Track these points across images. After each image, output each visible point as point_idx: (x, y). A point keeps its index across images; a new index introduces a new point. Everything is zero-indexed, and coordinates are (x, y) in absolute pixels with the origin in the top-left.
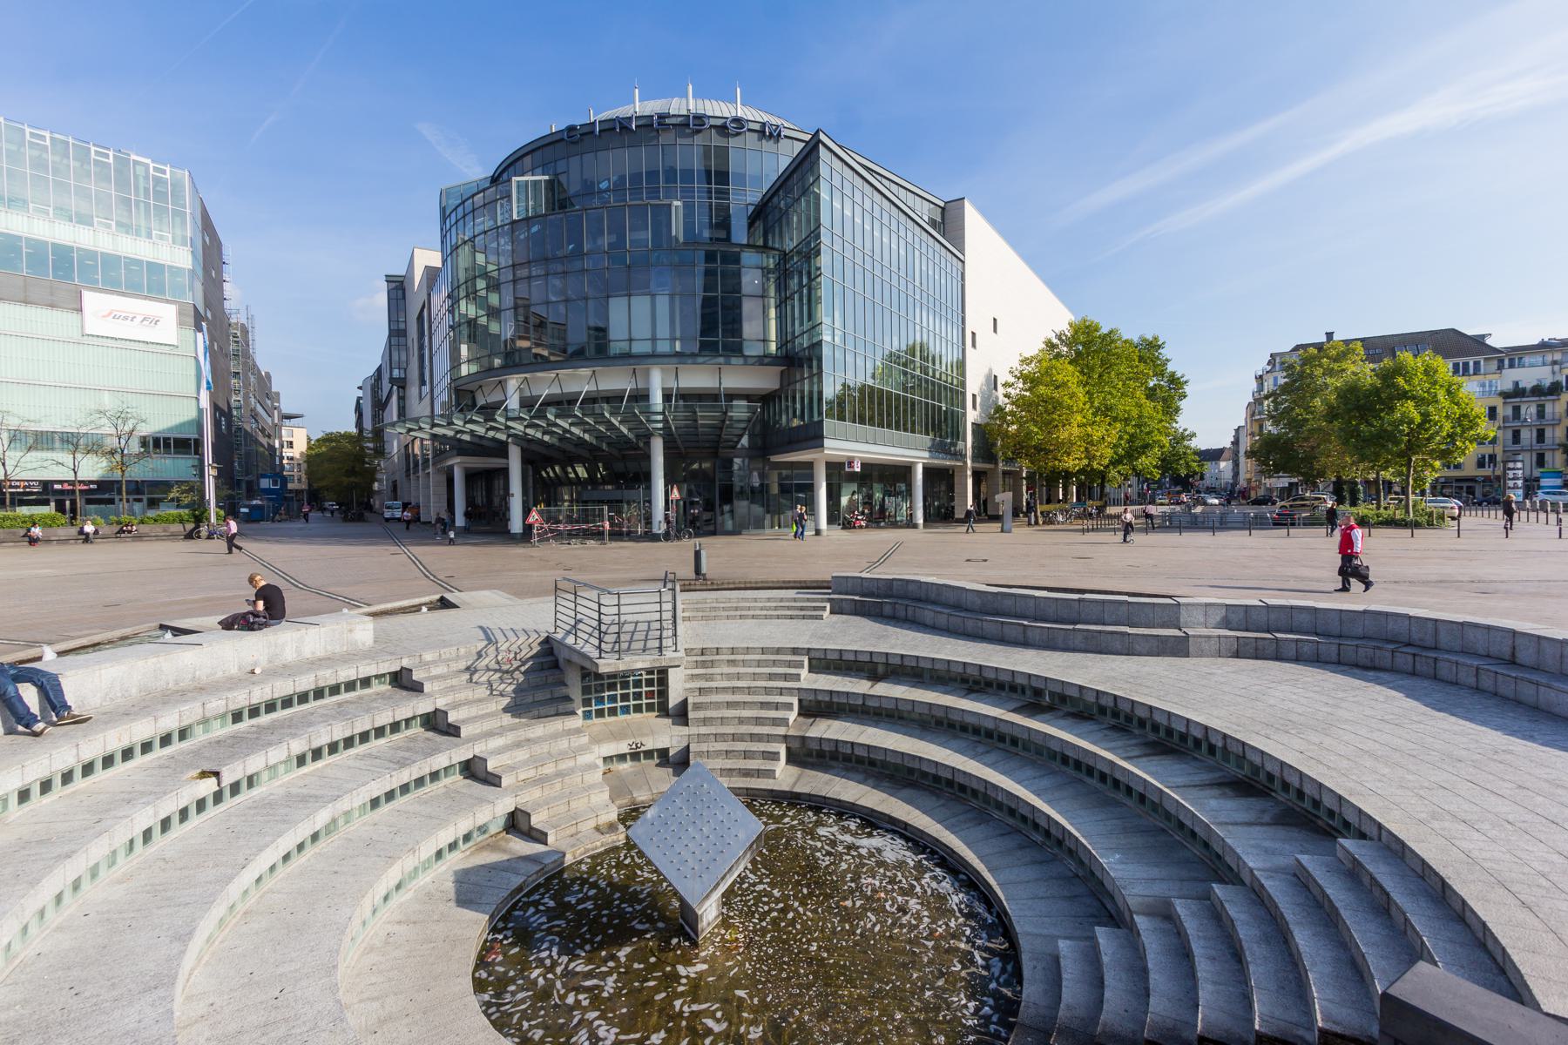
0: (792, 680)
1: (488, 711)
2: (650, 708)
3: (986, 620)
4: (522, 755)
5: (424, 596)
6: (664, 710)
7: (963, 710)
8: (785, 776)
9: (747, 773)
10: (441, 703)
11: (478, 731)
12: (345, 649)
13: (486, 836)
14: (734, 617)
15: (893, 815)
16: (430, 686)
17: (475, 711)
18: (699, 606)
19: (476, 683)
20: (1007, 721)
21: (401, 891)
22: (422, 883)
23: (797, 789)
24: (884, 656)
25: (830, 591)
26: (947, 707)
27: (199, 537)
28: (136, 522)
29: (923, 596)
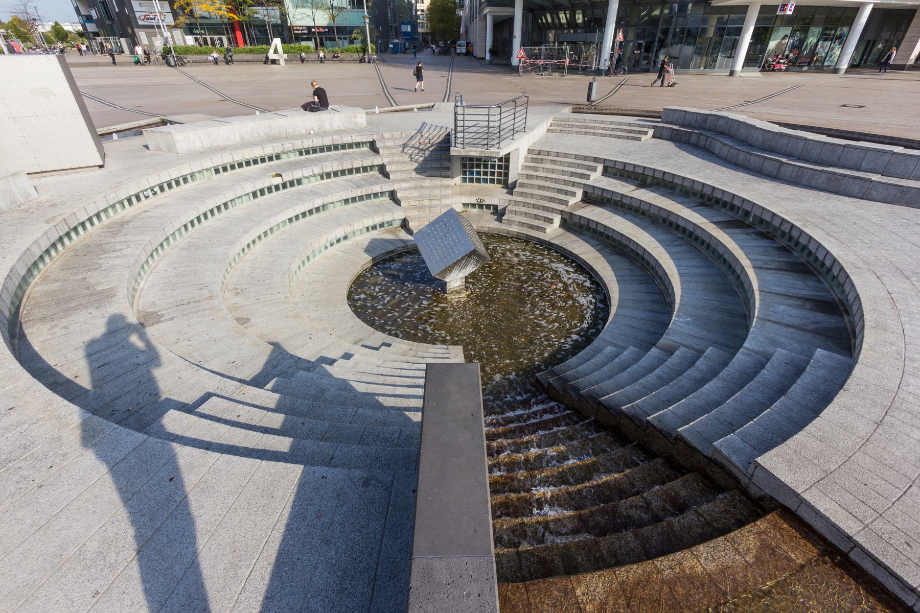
1: (407, 168)
2: (499, 182)
3: (754, 155)
4: (416, 193)
6: (505, 184)
7: (678, 216)
8: (553, 231)
9: (531, 227)
10: (385, 161)
11: (399, 178)
13: (391, 227)
14: (580, 133)
15: (593, 266)
17: (400, 167)
18: (563, 123)
20: (701, 228)
23: (552, 241)
24: (652, 171)
25: (660, 120)
26: (670, 212)
27: (365, 62)
28: (339, 51)
29: (726, 132)
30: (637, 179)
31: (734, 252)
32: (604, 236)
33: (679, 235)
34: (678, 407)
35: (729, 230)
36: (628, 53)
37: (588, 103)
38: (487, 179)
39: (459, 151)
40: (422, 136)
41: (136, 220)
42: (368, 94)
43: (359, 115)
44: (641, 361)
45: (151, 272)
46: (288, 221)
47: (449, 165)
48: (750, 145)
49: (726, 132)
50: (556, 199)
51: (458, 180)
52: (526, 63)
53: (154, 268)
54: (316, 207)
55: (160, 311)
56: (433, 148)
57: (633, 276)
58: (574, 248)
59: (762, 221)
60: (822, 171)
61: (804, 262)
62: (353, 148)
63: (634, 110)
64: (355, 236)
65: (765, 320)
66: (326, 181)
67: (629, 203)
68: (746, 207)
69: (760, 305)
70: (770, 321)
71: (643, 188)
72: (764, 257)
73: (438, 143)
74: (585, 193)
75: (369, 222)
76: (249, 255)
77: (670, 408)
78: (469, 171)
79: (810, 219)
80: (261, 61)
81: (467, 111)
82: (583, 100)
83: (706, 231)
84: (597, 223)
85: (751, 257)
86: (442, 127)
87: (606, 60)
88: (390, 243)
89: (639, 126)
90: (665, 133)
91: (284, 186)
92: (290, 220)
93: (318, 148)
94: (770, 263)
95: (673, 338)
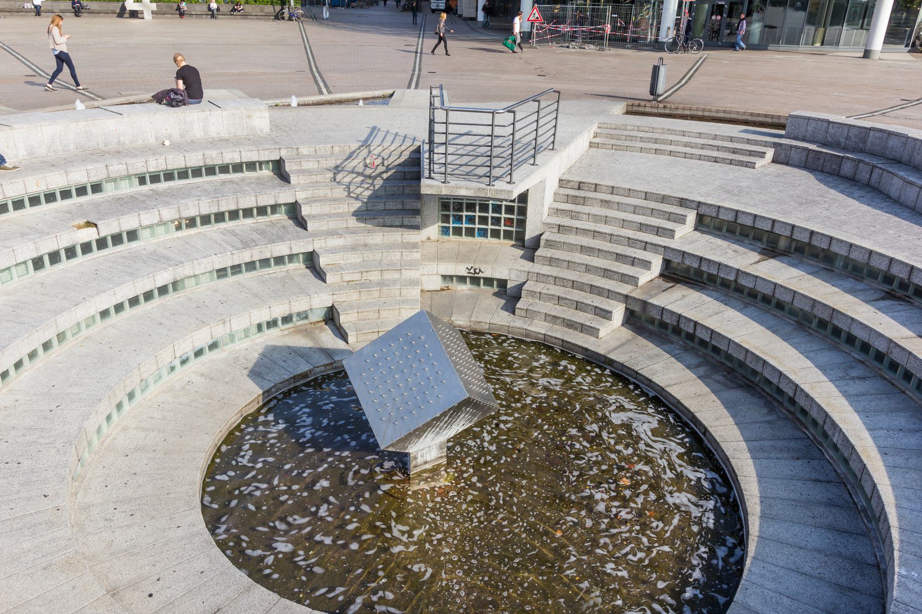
1: (340, 211)
2: (508, 235)
4: (355, 258)
5: (378, 90)
6: (520, 240)
7: (852, 319)
9: (571, 325)
10: (300, 196)
11: (325, 228)
12: (246, 133)
13: (305, 322)
14: (648, 151)
16: (296, 178)
17: (326, 209)
18: (617, 132)
19: (339, 183)
20: (904, 349)
21: (216, 351)
22: (237, 348)
23: (612, 356)
24: (790, 228)
25: (783, 132)
26: (834, 310)
27: (283, 18)
29: (905, 158)
30: (760, 240)
32: (710, 347)
33: (856, 356)
36: (703, 18)
37: (651, 97)
38: (487, 230)
39: (438, 187)
40: (370, 152)
42: (283, 71)
46: (98, 317)
47: (417, 205)
49: (903, 160)
50: (615, 272)
52: (542, 28)
54: (160, 285)
56: (389, 174)
57: (779, 439)
58: (655, 373)
63: (730, 112)
66: (186, 233)
67: (751, 285)
71: (773, 257)
73: (399, 165)
75: (264, 316)
80: (113, 12)
82: (643, 91)
83: (915, 357)
84: (696, 323)
86: (405, 137)
87: (669, 28)
89: (748, 141)
91: (102, 244)
92: (105, 314)
93: (176, 172)
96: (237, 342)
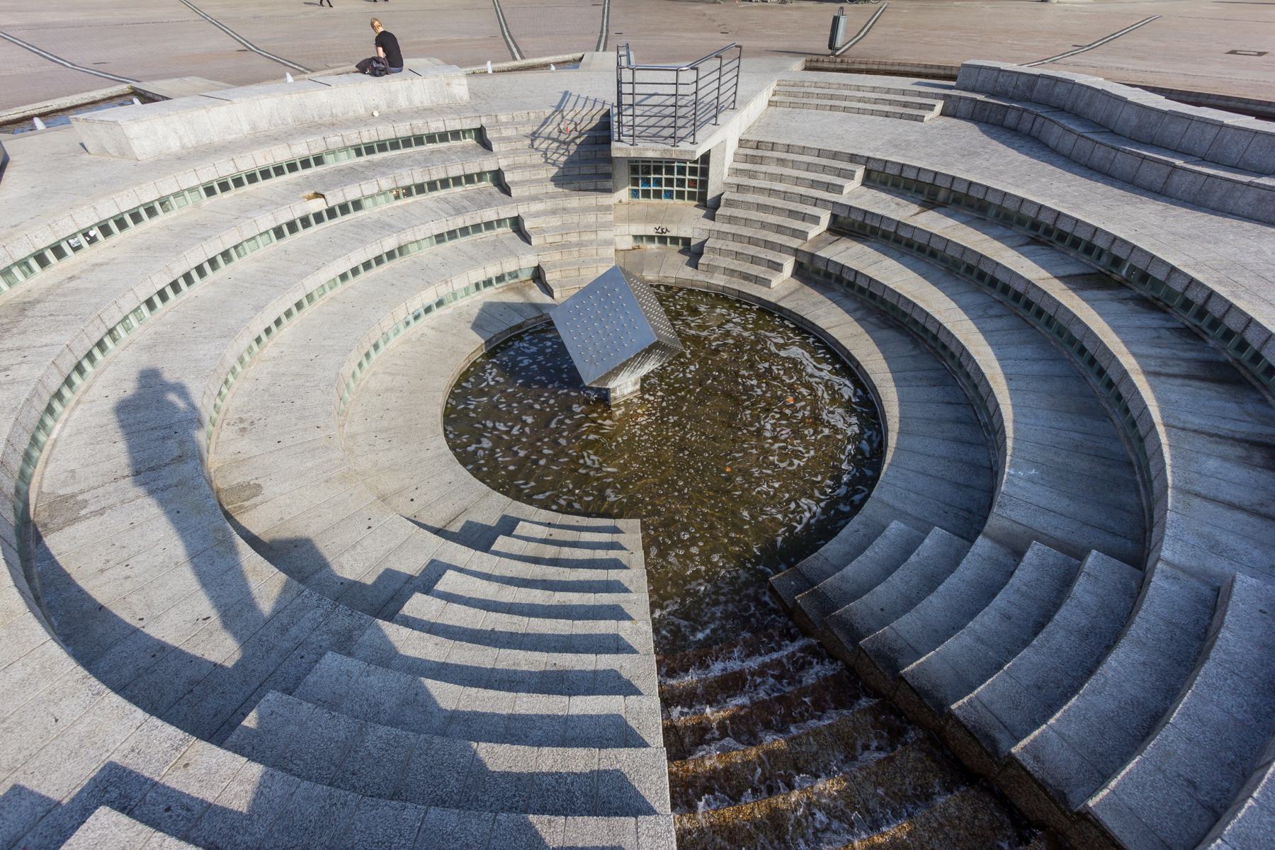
0: (833, 191)
2: (692, 196)
3: (1124, 151)
4: (555, 221)
6: (701, 199)
7: (997, 264)
9: (746, 277)
10: (503, 163)
11: (527, 194)
13: (516, 280)
15: (852, 352)
17: (527, 175)
18: (795, 89)
19: (536, 149)
20: (1040, 289)
23: (782, 304)
26: (982, 256)
30: (921, 192)
31: (1105, 341)
32: (867, 293)
34: (1066, 719)
35: (1089, 293)
39: (627, 149)
40: (563, 117)
41: (51, 297)
42: (477, 37)
43: (456, 81)
44: (961, 568)
45: (78, 402)
48: (1112, 131)
51: (624, 194)
53: (86, 391)
55: (82, 492)
56: (582, 139)
59: (1144, 277)
60: (1249, 184)
61: (1230, 360)
62: (447, 141)
63: (905, 65)
64: (455, 299)
65: (1188, 492)
68: (1117, 251)
69: (1173, 457)
70: (1197, 495)
71: (932, 209)
72: (1158, 350)
73: (591, 130)
74: (834, 217)
75: (479, 275)
76: (270, 348)
77: (1052, 721)
78: (643, 179)
79: (1241, 280)
81: (640, 76)
82: (822, 45)
83: (1049, 296)
84: (857, 272)
85: (1135, 349)
86: (595, 101)
88: (515, 310)
89: (920, 94)
90: (963, 107)
91: (331, 213)
92: (343, 277)
94: (1170, 363)
95: (1013, 515)
96: (460, 300)
